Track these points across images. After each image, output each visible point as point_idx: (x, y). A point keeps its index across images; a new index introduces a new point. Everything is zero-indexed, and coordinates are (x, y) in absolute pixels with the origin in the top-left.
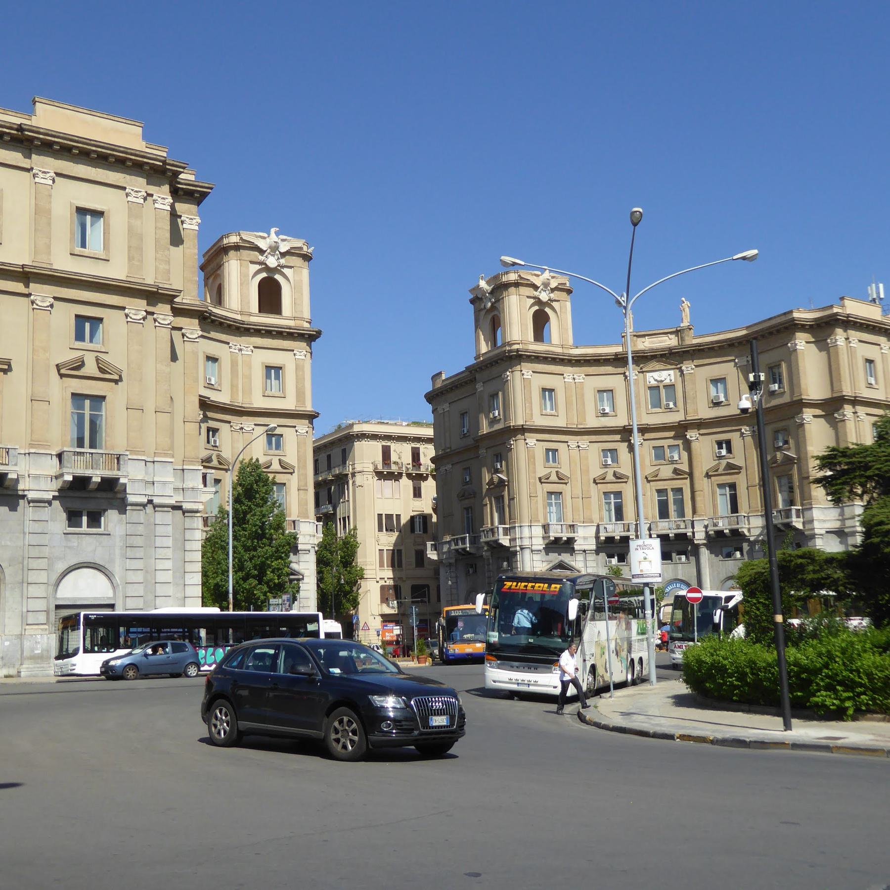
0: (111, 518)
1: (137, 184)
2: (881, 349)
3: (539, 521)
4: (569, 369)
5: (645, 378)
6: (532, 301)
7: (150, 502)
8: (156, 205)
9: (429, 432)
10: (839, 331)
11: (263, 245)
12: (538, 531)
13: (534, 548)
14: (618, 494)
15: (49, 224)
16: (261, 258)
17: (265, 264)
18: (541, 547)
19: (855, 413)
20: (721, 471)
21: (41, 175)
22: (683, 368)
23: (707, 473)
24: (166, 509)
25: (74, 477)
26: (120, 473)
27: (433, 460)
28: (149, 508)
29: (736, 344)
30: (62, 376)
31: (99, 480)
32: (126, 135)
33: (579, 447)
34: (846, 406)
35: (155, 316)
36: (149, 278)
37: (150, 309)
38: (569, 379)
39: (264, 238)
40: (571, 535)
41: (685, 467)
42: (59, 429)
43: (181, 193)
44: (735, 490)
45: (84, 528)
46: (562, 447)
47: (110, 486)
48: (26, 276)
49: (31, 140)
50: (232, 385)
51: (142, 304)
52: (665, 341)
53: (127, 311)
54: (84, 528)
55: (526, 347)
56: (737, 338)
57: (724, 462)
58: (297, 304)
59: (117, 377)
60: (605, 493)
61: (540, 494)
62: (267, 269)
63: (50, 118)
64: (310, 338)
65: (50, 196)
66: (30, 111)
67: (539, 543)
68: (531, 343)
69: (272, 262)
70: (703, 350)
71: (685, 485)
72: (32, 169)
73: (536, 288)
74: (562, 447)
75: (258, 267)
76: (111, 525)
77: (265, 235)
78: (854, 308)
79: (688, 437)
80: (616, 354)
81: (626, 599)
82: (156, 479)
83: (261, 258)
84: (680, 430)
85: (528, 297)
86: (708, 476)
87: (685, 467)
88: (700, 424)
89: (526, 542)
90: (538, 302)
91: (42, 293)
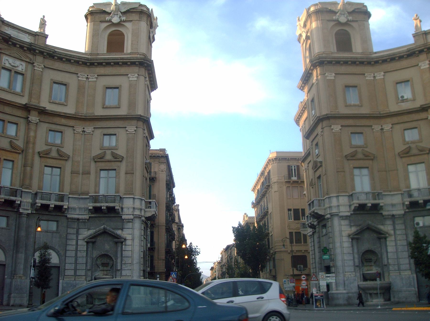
20: (360, 156)
83: (108, 18)
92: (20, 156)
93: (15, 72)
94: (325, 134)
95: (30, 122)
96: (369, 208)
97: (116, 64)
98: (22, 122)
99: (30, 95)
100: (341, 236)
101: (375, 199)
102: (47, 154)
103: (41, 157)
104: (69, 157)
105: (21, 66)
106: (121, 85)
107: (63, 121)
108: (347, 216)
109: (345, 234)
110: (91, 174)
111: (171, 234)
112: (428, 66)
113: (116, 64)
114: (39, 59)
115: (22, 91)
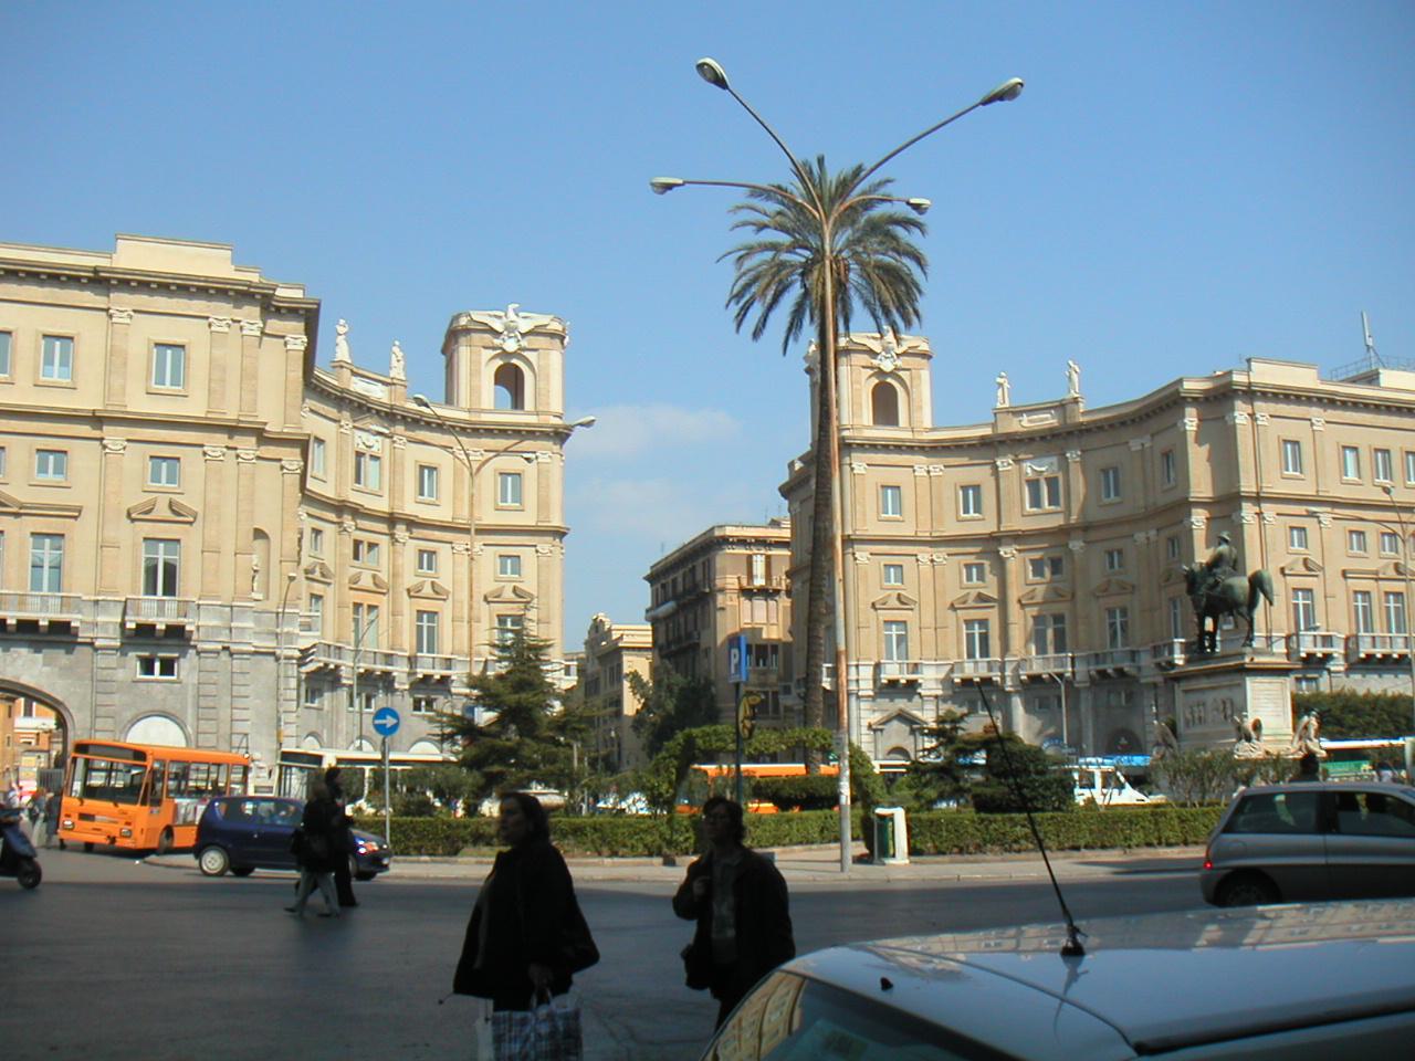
0: (186, 666)
1: (222, 311)
2: (1312, 424)
3: (870, 659)
4: (922, 458)
5: (1020, 468)
6: (870, 372)
7: (225, 648)
8: (244, 332)
9: (785, 533)
10: (1239, 404)
11: (498, 326)
12: (867, 673)
13: (860, 693)
14: (983, 623)
15: (125, 364)
16: (497, 342)
17: (501, 348)
18: (1342, 669)
19: (1259, 514)
20: (970, 603)
21: (119, 314)
22: (999, 463)
23: (952, 605)
24: (245, 656)
25: (138, 625)
26: (186, 620)
27: (788, 575)
28: (224, 656)
29: (1129, 422)
30: (133, 520)
31: (163, 627)
32: (214, 264)
33: (932, 561)
34: (1244, 505)
35: (238, 451)
36: (231, 414)
37: (231, 444)
38: (921, 472)
39: (500, 317)
40: (1327, 650)
41: (993, 592)
42: (127, 579)
43: (283, 311)
44: (986, 627)
45: (157, 675)
46: (907, 562)
47: (177, 634)
48: (97, 420)
49: (108, 280)
50: (455, 498)
51: (222, 439)
52: (1046, 419)
53: (205, 449)
54: (157, 675)
55: (856, 434)
56: (1106, 419)
57: (974, 593)
58: (548, 393)
59: (191, 519)
60: (967, 622)
61: (873, 624)
62: (505, 354)
63: (132, 256)
64: (560, 435)
65: (127, 334)
66: (110, 250)
67: (867, 687)
68: (868, 427)
69: (511, 346)
70: (961, 446)
71: (993, 615)
72: (109, 309)
73: (872, 353)
74: (907, 562)
75: (492, 353)
76: (183, 674)
77: (502, 314)
78: (1265, 374)
79: (1002, 553)
80: (982, 437)
81: (358, 766)
82: (233, 625)
83: (497, 342)
84: (992, 542)
85: (864, 367)
86: (953, 607)
87: (993, 592)
88: (1017, 537)
89: (853, 687)
90: (880, 373)
91: (114, 436)
92: (385, 598)
93: (371, 456)
94: (829, 556)
95: (397, 541)
96: (162, 634)
97: (441, 426)
98: (384, 541)
99: (392, 496)
100: (860, 725)
101: (913, 673)
102: (498, 596)
103: (411, 597)
104: (447, 593)
105: (376, 445)
106: (523, 471)
107: (437, 534)
108: (869, 696)
109: (865, 723)
110: (482, 620)
111: (441, 703)
112: (1195, 429)
113: (441, 426)
114: (400, 429)
115: (380, 488)
